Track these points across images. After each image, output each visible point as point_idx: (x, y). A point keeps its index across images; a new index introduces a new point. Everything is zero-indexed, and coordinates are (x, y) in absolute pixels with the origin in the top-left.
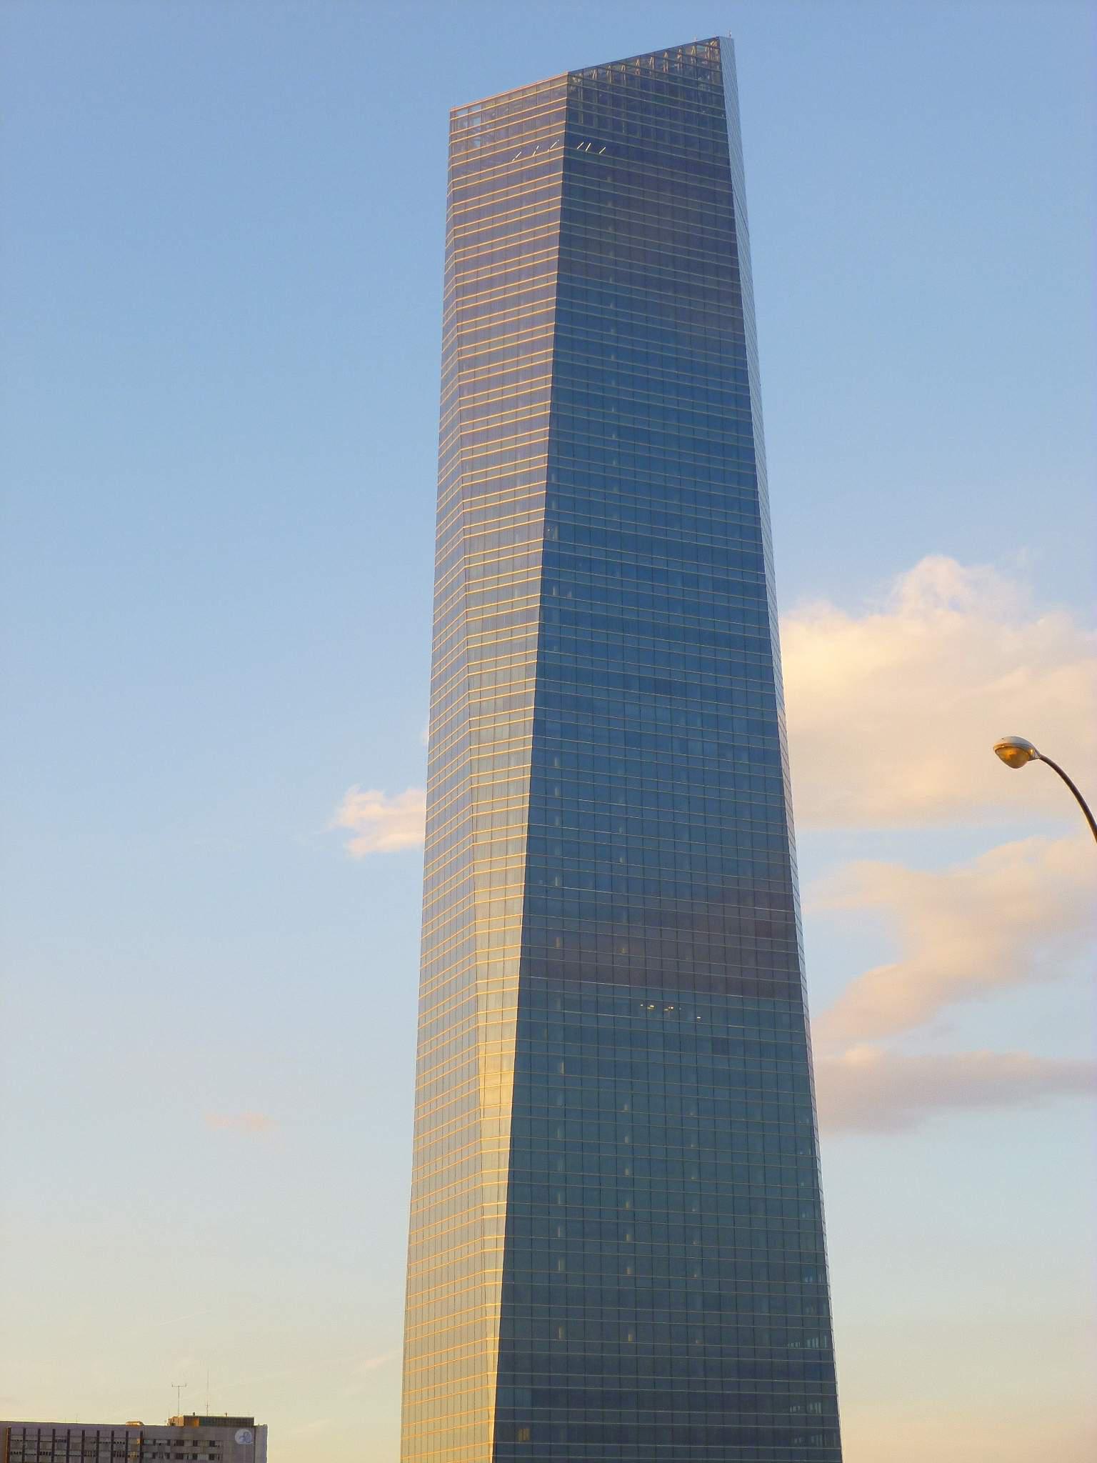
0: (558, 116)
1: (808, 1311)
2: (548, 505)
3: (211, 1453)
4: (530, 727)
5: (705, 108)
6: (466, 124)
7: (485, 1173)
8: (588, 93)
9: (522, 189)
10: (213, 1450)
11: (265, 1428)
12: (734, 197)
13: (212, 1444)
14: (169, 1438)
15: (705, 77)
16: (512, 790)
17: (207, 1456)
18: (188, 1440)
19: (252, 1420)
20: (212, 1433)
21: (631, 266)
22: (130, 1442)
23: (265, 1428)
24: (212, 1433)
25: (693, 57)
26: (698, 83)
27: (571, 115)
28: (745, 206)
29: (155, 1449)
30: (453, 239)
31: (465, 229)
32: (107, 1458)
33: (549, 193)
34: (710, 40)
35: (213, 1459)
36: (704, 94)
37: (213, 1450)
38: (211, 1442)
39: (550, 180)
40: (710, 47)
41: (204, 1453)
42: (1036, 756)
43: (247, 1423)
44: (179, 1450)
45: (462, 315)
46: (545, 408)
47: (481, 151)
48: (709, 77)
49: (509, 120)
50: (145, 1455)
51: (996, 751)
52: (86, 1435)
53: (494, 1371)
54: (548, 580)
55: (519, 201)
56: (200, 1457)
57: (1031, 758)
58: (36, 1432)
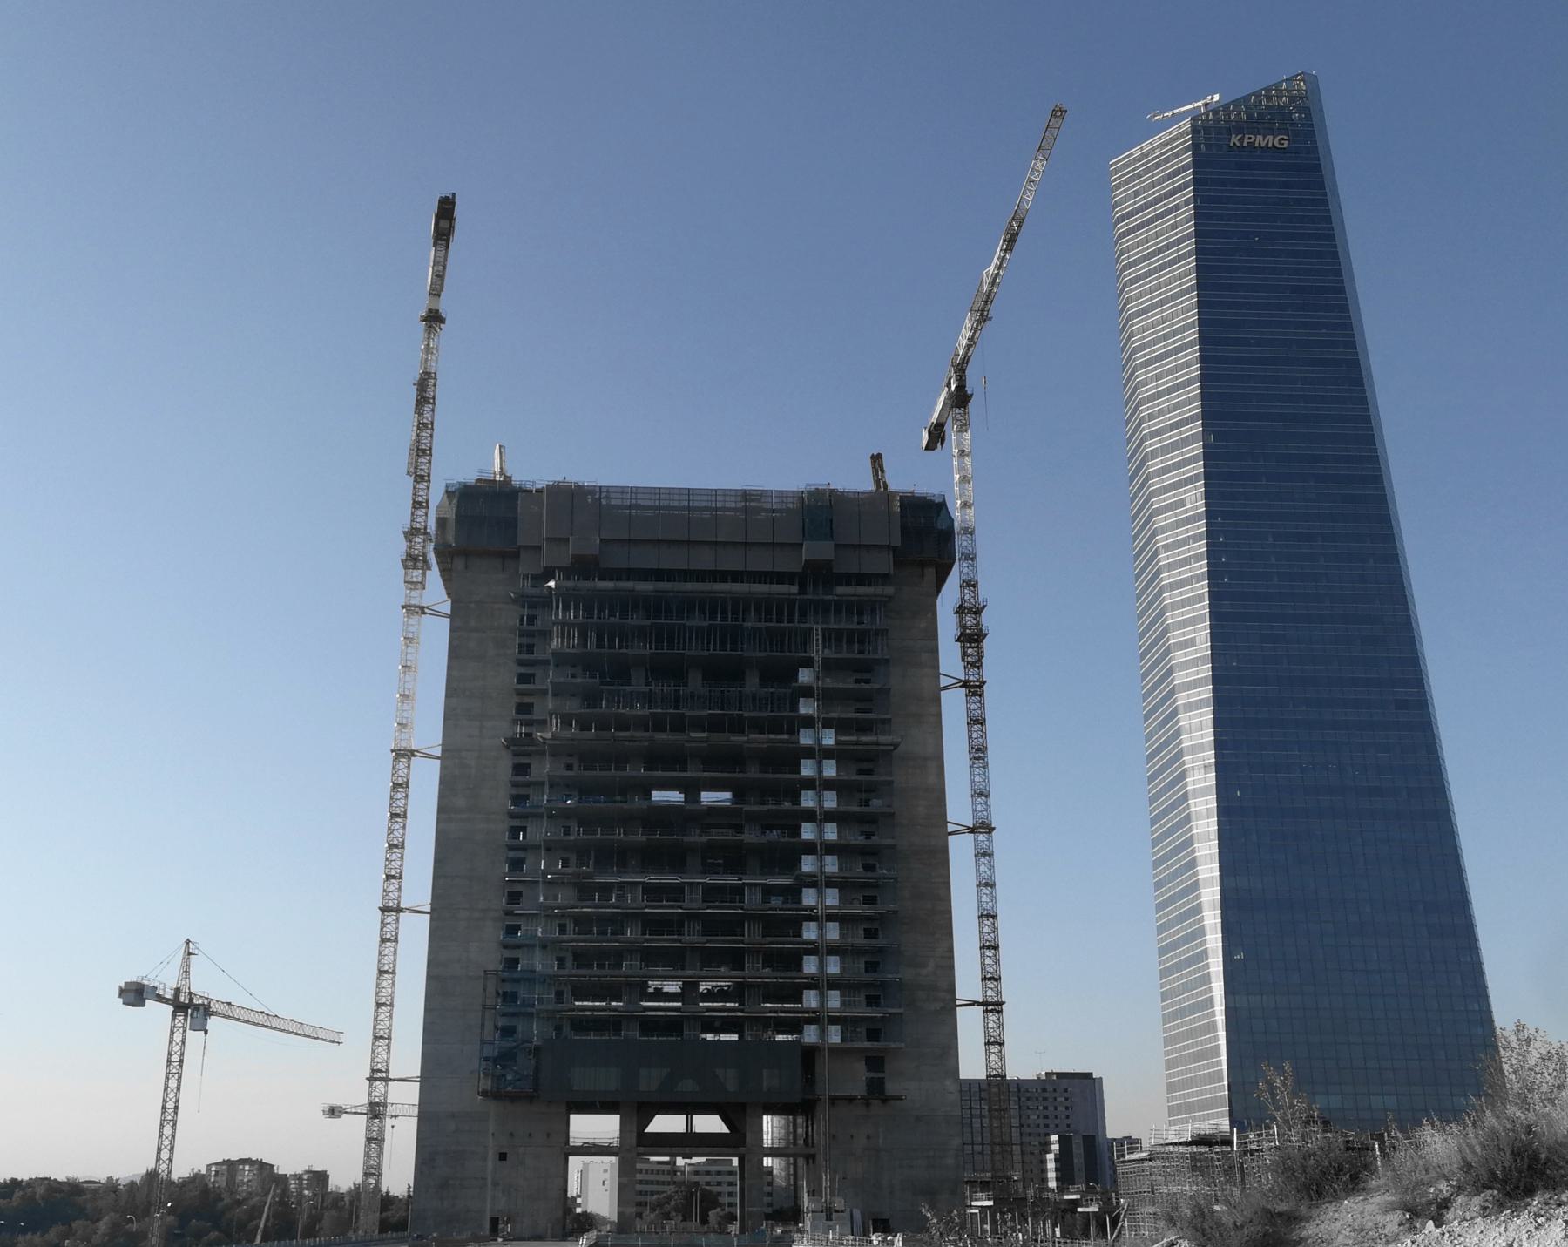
0: (1186, 150)
4: (1210, 723)
7: (1204, 879)
8: (1206, 130)
10: (1066, 1095)
11: (1101, 1078)
19: (1091, 1074)
20: (1065, 1083)
22: (972, 1090)
23: (1101, 1078)
24: (1065, 1083)
27: (1195, 147)
29: (1028, 1095)
35: (505, 1159)
37: (1066, 1095)
41: (1061, 1096)
43: (1088, 1076)
46: (1194, 333)
53: (1222, 1006)
54: (1216, 654)
58: (1016, 1086)
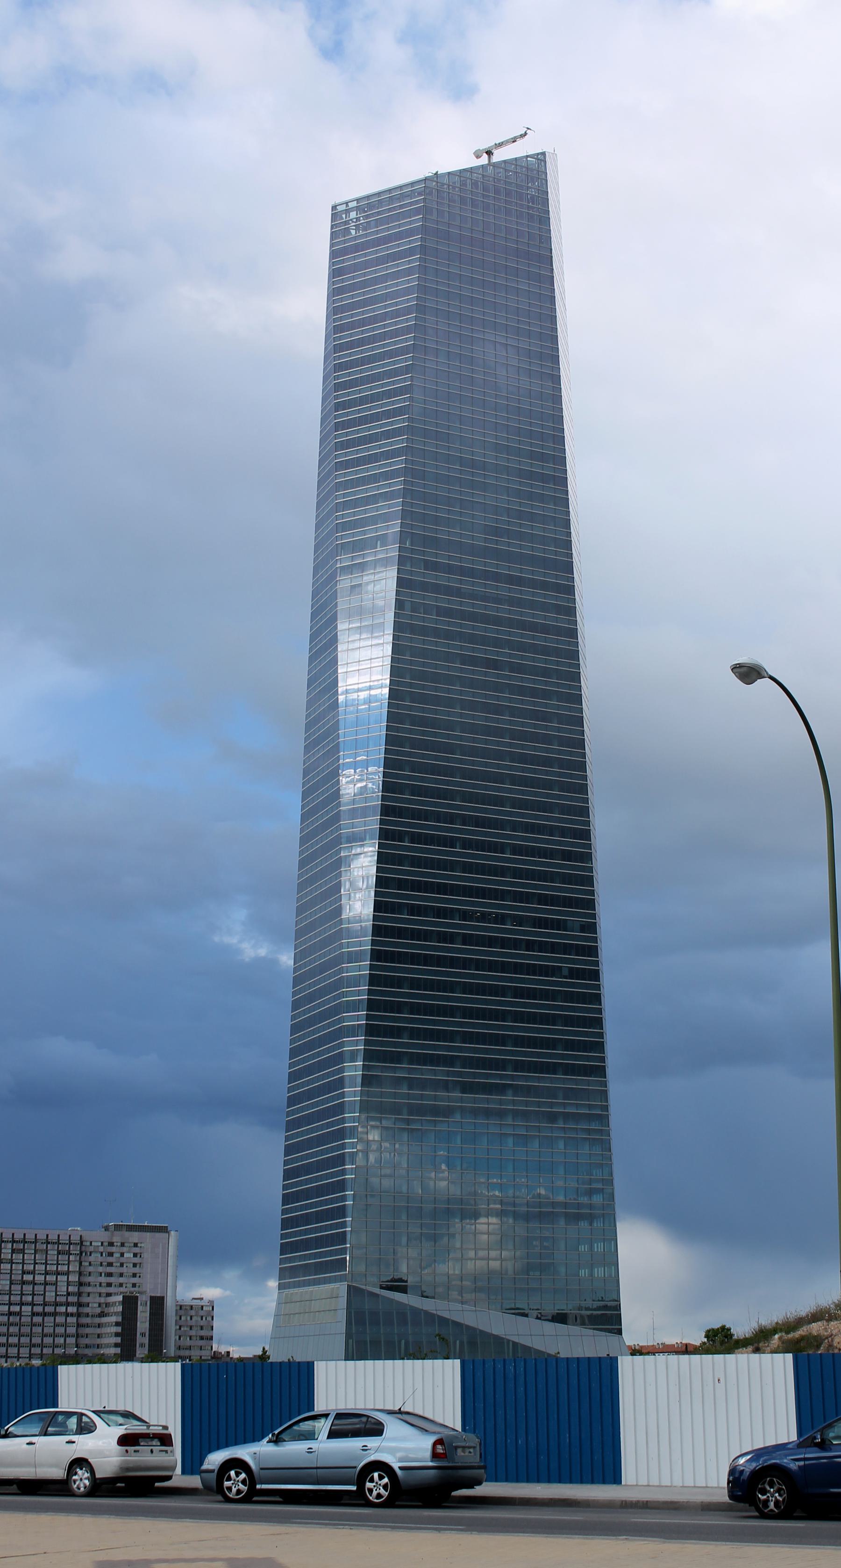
1: (594, 1174)
2: (402, 541)
3: (134, 1282)
5: (533, 208)
6: (344, 216)
9: (387, 268)
10: (136, 1250)
12: (555, 278)
13: (136, 1245)
14: (102, 1241)
15: (535, 184)
16: (371, 743)
17: (132, 1255)
18: (117, 1252)
21: (484, 435)
25: (525, 167)
26: (528, 188)
28: (563, 287)
30: (333, 364)
31: (342, 300)
32: (53, 1296)
33: (409, 272)
34: (538, 154)
36: (533, 197)
37: (136, 1250)
38: (134, 1243)
39: (408, 281)
40: (538, 159)
41: (129, 1252)
42: (766, 675)
44: (110, 1259)
45: (338, 407)
47: (355, 238)
48: (536, 184)
49: (379, 213)
50: (83, 1263)
51: (732, 670)
52: (38, 1238)
55: (385, 278)
56: (126, 1255)
57: (761, 676)
